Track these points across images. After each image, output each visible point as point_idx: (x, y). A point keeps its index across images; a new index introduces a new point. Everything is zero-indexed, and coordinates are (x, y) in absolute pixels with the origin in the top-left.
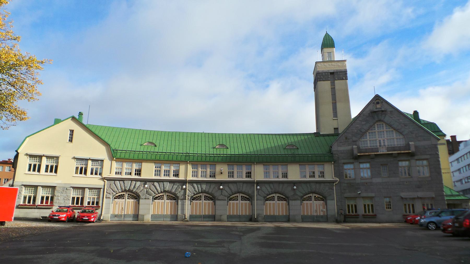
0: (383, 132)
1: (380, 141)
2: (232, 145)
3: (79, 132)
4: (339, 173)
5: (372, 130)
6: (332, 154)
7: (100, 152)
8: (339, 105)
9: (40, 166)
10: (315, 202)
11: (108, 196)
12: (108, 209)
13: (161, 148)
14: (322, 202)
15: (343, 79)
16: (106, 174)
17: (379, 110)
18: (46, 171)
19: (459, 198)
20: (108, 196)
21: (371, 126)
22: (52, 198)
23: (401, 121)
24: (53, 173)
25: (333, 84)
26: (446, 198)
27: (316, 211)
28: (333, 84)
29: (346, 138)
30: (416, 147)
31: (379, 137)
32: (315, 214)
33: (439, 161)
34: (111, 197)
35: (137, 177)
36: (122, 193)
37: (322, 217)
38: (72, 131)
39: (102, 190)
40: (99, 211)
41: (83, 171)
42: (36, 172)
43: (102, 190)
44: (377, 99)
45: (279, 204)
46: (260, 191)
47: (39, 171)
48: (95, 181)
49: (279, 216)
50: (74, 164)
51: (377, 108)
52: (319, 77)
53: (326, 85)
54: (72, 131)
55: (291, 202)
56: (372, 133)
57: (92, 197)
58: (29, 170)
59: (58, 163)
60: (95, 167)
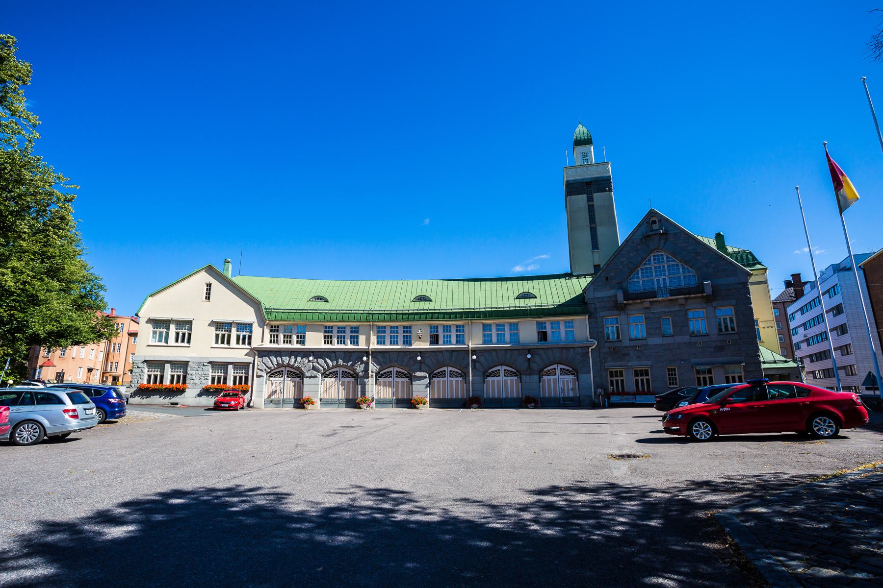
0: (664, 267)
1: (658, 280)
2: (439, 296)
3: (216, 286)
4: (596, 331)
5: (645, 264)
6: (586, 303)
7: (247, 315)
8: (600, 231)
9: (229, 336)
10: (561, 377)
11: (260, 373)
12: (260, 391)
13: (438, 303)
14: (572, 377)
15: (605, 191)
16: (256, 343)
17: (656, 232)
18: (238, 343)
19: (786, 365)
20: (260, 373)
21: (643, 259)
22: (185, 377)
23: (689, 248)
24: (185, 344)
25: (590, 199)
26: (763, 366)
27: (563, 391)
28: (590, 199)
29: (607, 279)
30: (714, 286)
31: (657, 276)
32: (562, 395)
33: (751, 309)
34: (264, 374)
35: (299, 346)
36: (334, 370)
37: (572, 399)
38: (209, 285)
39: (251, 365)
40: (247, 396)
41: (224, 340)
42: (225, 346)
43: (251, 365)
44: (652, 218)
45: (506, 381)
46: (477, 364)
47: (229, 343)
48: (237, 353)
49: (506, 399)
50: (213, 330)
51: (652, 231)
52: (573, 188)
53: (581, 200)
54: (209, 285)
55: (524, 377)
56: (646, 269)
57: (238, 375)
58: (217, 342)
59: (190, 329)
60: (241, 334)
